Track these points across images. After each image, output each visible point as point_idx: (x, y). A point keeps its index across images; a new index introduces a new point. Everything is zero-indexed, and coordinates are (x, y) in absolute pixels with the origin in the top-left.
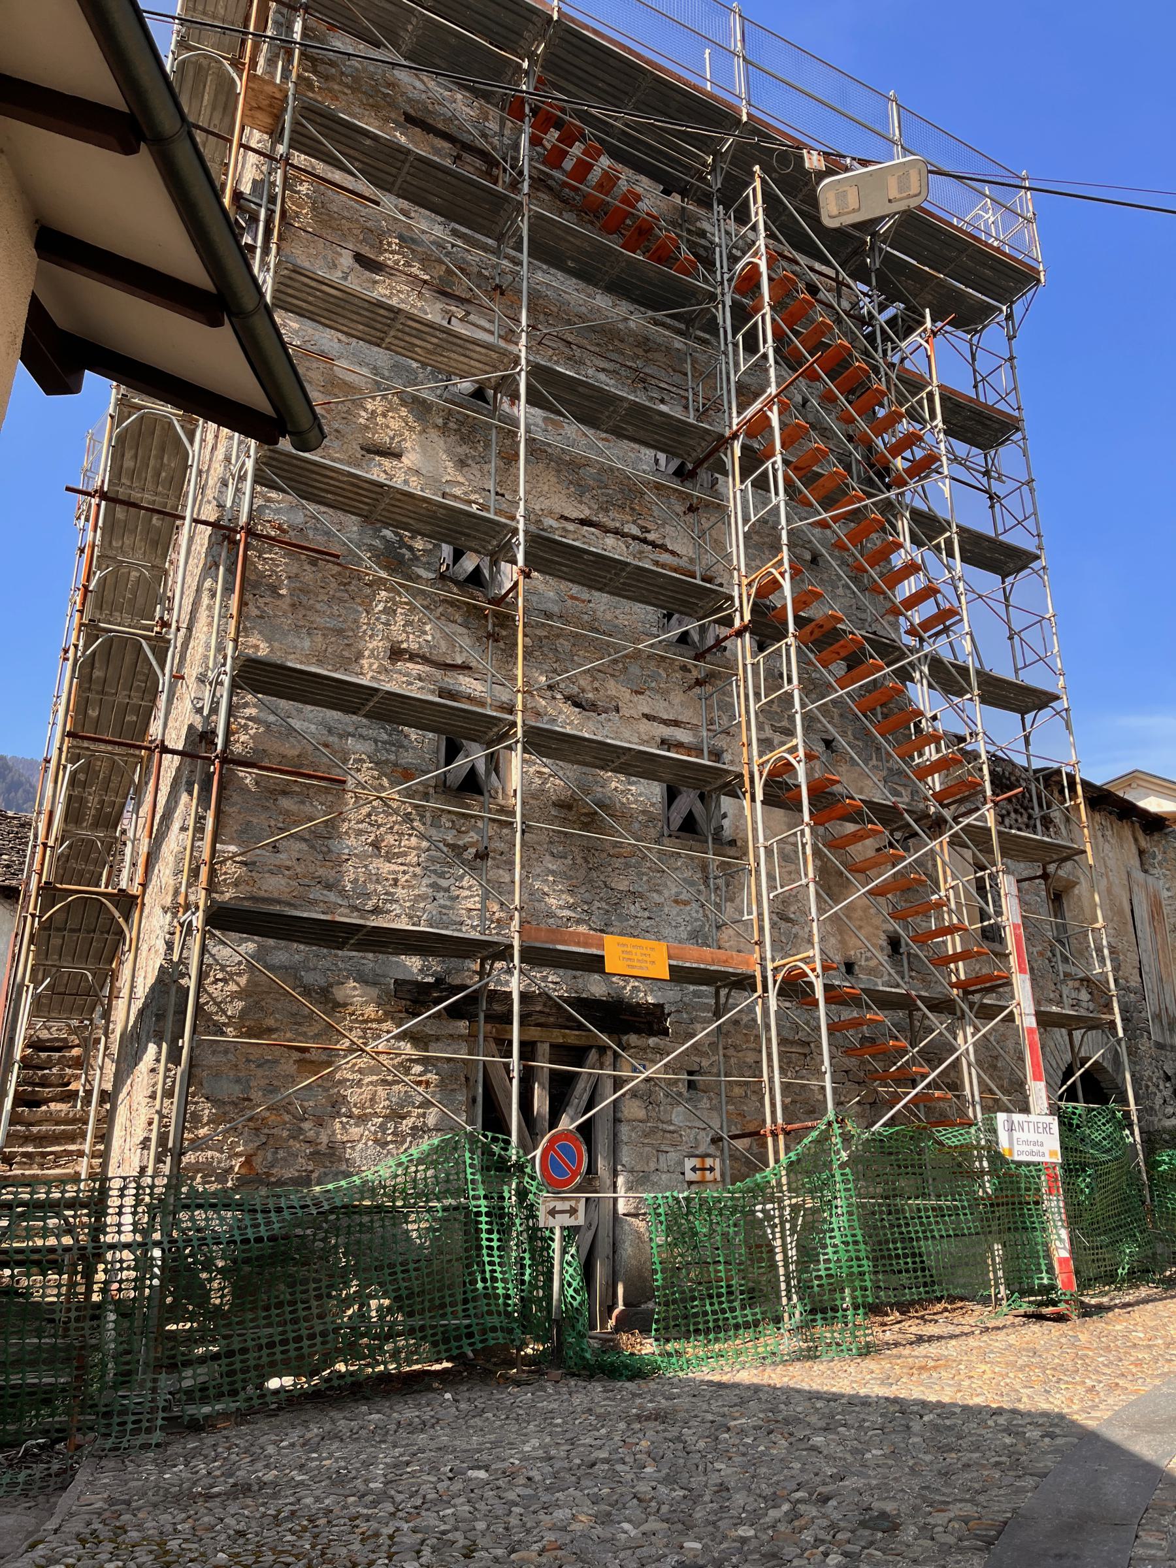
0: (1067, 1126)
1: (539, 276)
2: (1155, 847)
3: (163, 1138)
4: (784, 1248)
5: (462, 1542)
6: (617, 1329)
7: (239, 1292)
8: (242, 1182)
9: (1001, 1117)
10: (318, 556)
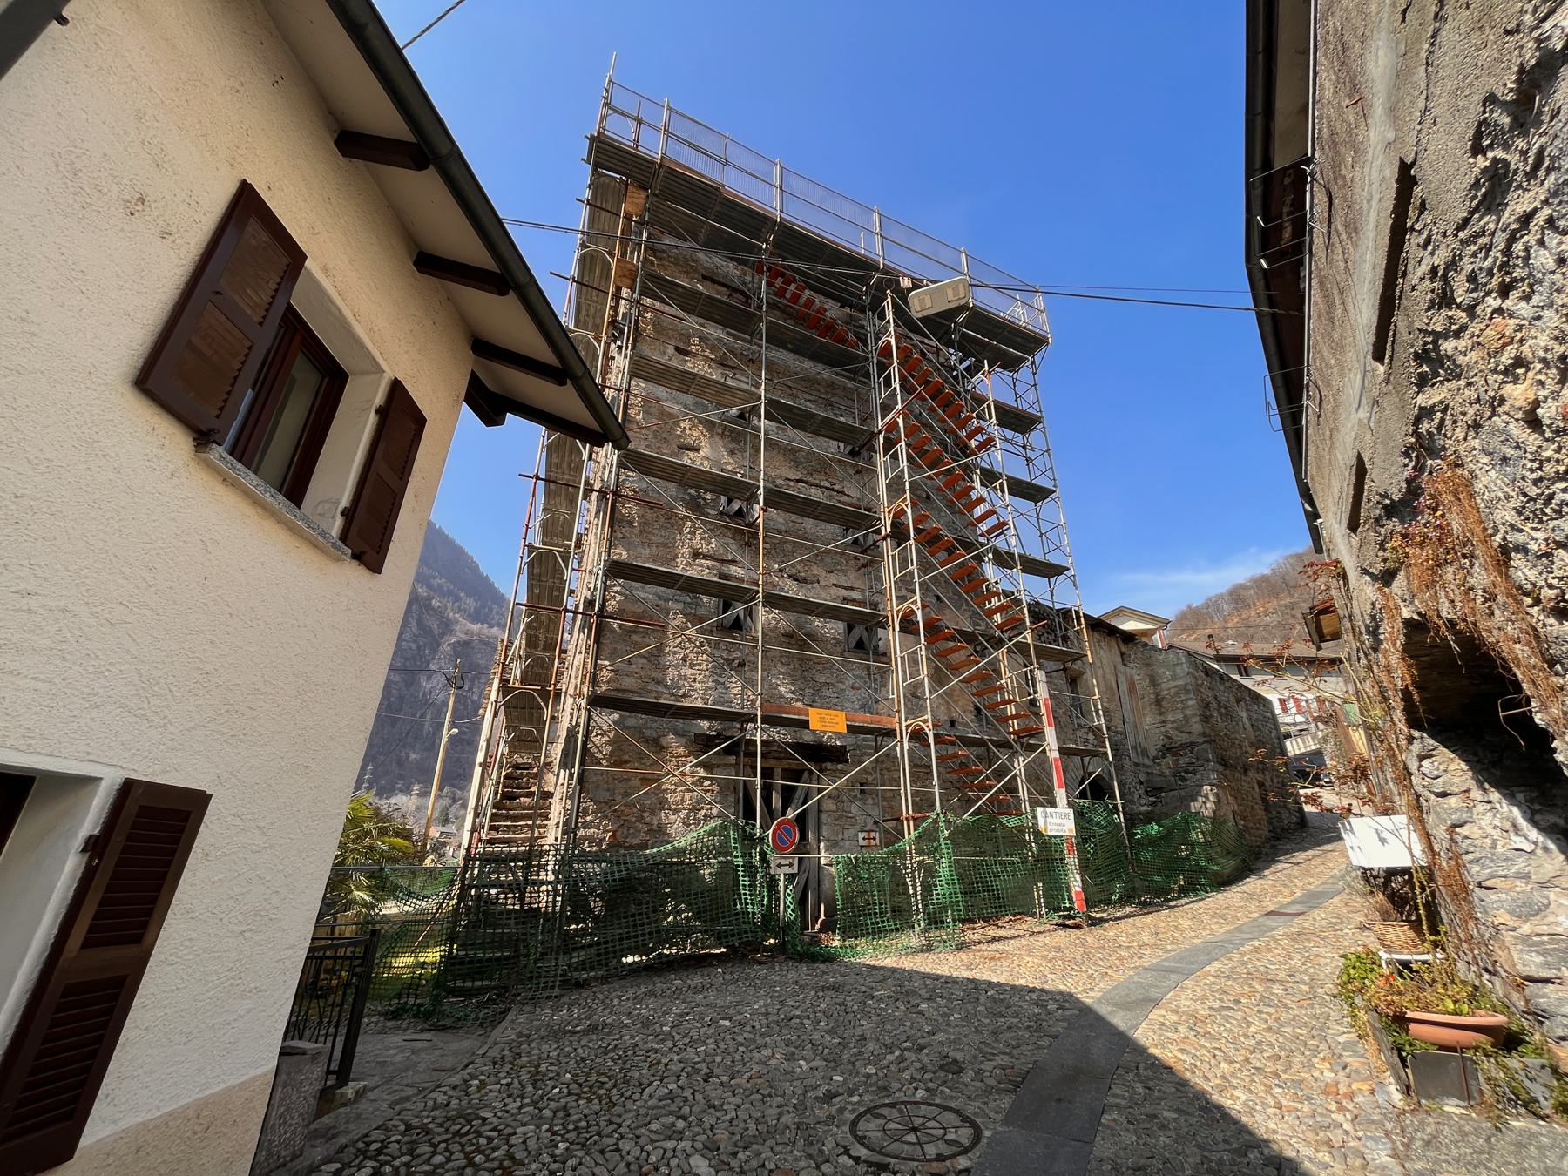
0: (1080, 815)
1: (774, 353)
2: (1131, 652)
3: (565, 824)
4: (914, 887)
5: (705, 1070)
6: (821, 931)
7: (609, 907)
8: (610, 846)
9: (1040, 810)
10: (655, 506)
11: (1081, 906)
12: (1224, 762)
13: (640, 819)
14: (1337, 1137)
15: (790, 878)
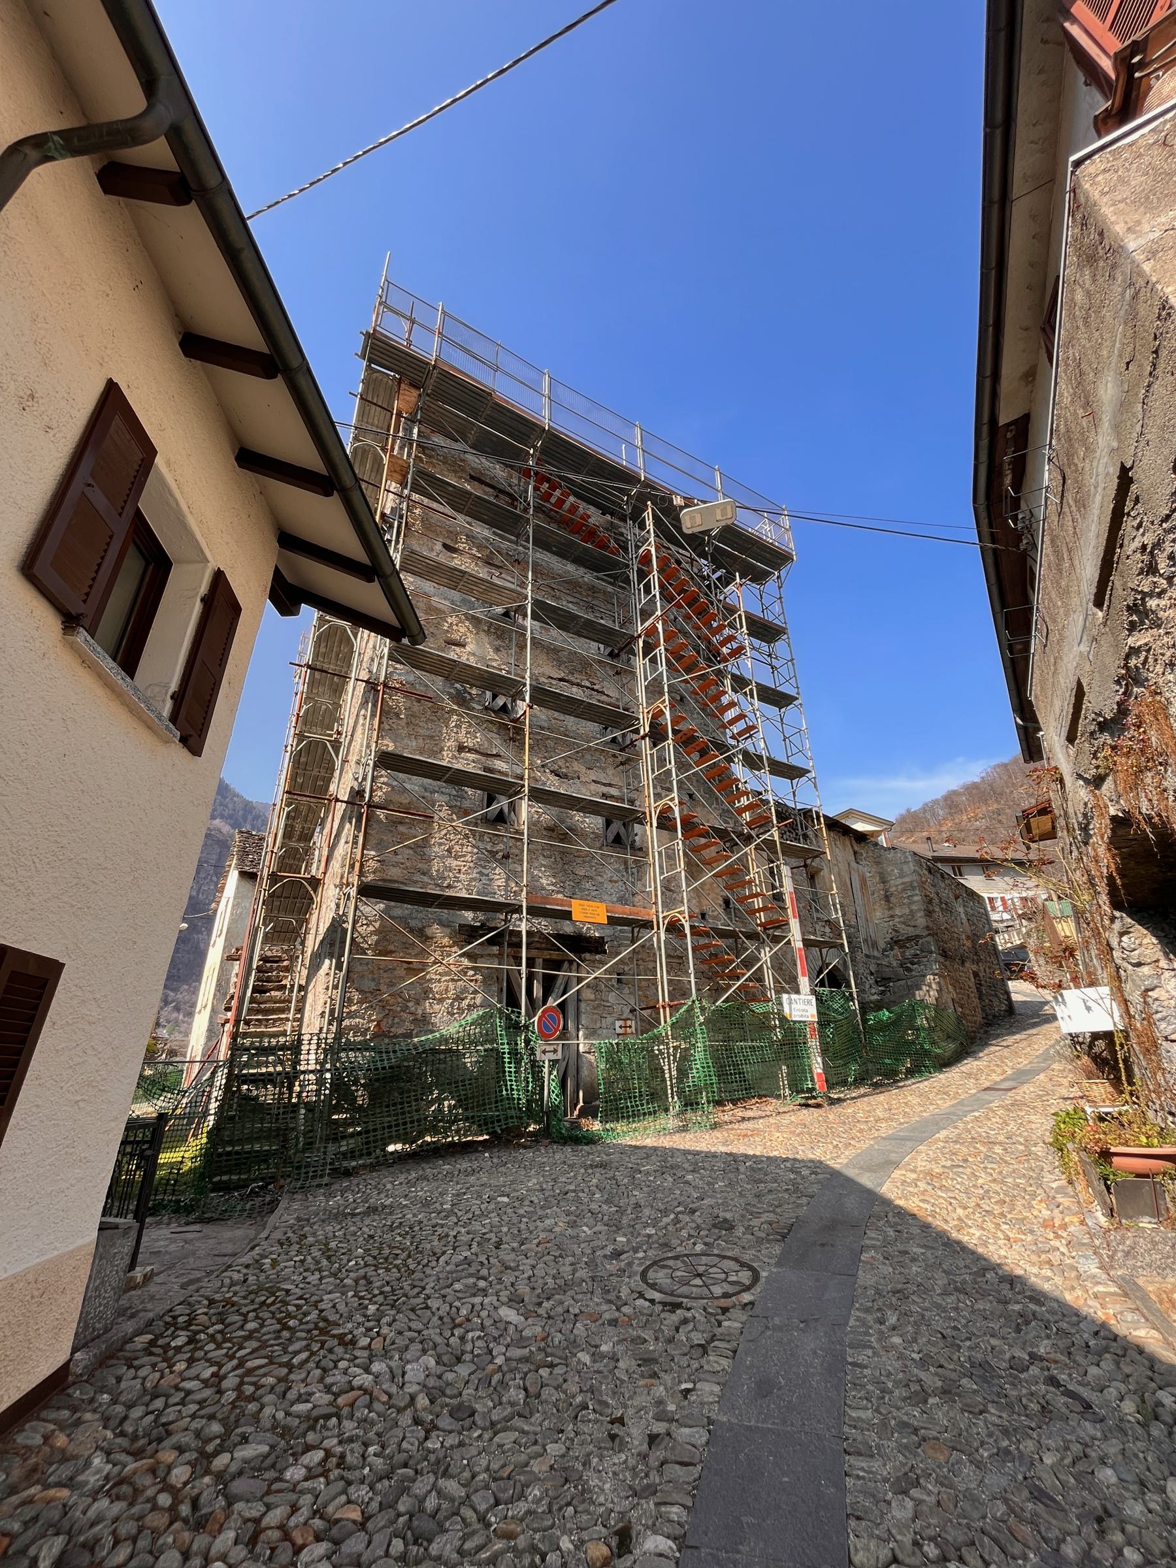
0: (820, 1001)
1: (538, 555)
2: (862, 850)
3: (332, 1011)
4: (670, 1070)
5: (494, 1239)
6: (579, 1116)
8: (375, 1036)
9: (785, 996)
10: (421, 698)
11: (821, 1087)
12: (944, 954)
13: (405, 1009)
14: (1055, 1258)
15: (553, 1063)
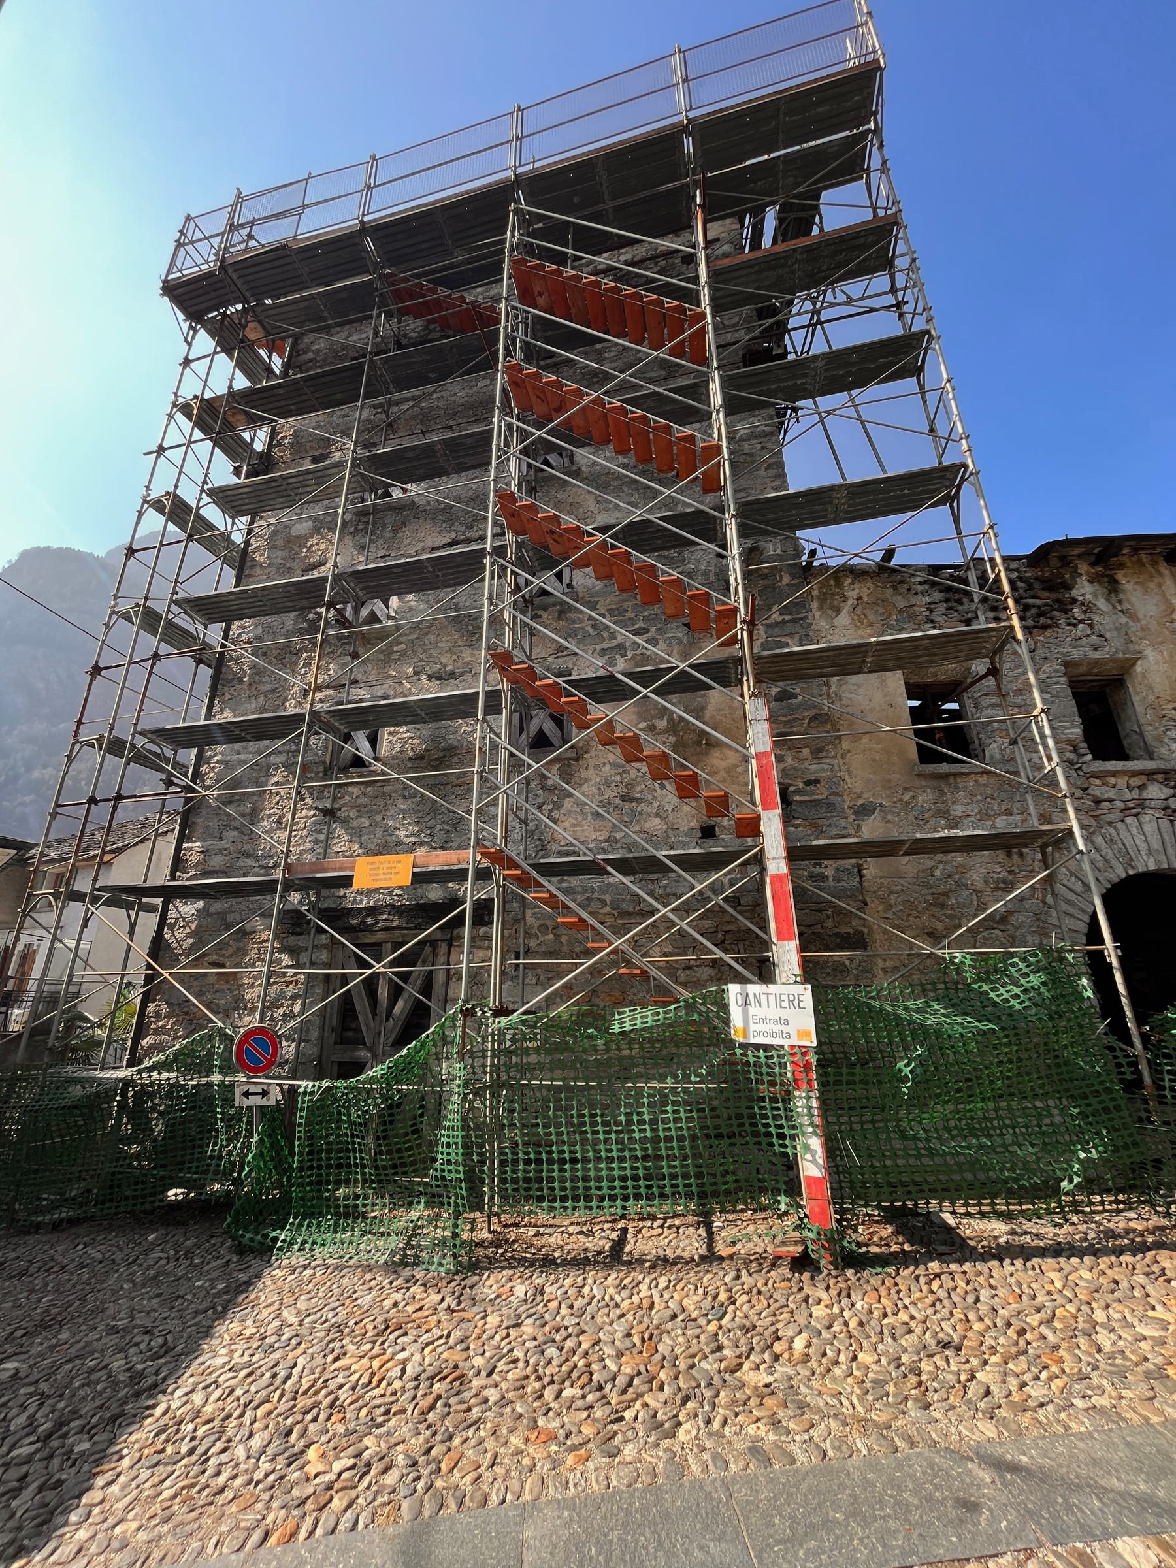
9: (734, 989)
